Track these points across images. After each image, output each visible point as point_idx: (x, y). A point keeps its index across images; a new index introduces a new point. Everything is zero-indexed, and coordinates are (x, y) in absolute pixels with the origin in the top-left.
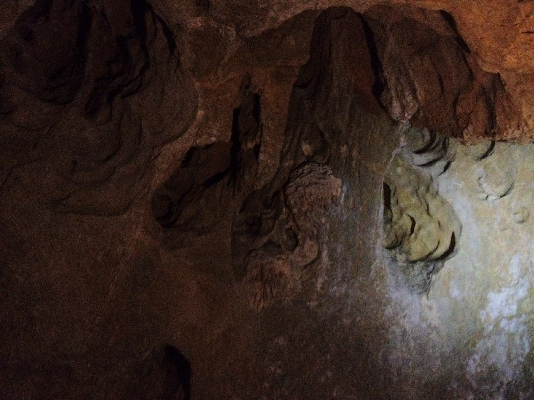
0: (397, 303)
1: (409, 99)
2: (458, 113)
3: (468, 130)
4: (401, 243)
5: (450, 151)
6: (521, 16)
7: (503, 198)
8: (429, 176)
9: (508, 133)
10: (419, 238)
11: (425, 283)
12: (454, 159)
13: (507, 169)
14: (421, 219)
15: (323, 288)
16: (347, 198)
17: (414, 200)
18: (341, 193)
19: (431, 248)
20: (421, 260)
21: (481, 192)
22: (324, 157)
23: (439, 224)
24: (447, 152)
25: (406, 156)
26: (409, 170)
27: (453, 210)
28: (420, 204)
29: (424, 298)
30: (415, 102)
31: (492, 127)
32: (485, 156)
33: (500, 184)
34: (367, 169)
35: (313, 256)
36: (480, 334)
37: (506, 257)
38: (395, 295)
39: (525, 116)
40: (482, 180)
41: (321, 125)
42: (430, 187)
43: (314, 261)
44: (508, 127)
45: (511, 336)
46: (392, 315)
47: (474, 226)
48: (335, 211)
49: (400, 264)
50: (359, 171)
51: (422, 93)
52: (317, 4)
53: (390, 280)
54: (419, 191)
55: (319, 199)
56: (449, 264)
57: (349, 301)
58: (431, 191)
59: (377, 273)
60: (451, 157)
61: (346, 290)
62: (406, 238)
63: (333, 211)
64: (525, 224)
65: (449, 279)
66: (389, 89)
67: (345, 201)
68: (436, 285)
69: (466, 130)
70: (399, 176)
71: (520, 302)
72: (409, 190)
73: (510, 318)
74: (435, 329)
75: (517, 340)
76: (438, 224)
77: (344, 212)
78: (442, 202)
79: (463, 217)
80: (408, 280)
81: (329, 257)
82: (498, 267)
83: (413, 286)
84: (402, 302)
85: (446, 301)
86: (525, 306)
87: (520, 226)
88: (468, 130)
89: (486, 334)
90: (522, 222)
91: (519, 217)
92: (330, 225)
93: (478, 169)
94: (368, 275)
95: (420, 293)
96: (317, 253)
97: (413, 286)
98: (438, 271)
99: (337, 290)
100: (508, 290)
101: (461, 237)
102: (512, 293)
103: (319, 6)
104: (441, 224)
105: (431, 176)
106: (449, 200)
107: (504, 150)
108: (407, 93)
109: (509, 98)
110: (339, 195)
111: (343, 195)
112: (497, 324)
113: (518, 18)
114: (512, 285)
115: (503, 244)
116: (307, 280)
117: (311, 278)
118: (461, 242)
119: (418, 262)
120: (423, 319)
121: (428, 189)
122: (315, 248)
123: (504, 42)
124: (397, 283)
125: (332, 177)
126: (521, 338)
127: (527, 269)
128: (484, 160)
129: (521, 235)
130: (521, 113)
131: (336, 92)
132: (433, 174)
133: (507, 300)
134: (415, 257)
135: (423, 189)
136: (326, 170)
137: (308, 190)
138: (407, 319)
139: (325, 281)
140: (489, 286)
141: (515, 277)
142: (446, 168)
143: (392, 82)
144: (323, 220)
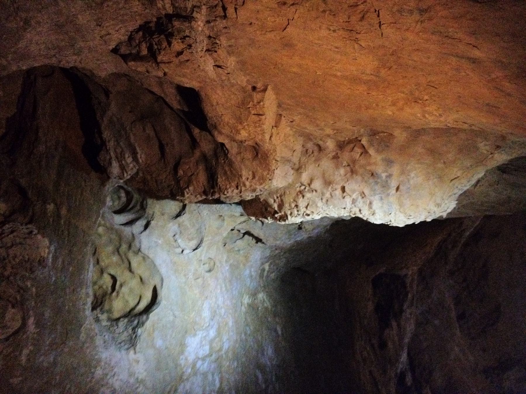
0: (106, 363)
1: (129, 160)
2: (179, 174)
3: (189, 190)
4: (101, 303)
5: (149, 211)
6: (253, 102)
7: (195, 251)
8: (130, 233)
9: (228, 192)
10: (121, 295)
11: (131, 338)
12: (152, 218)
13: (197, 226)
14: (122, 276)
15: (29, 360)
16: (55, 258)
17: (115, 259)
18: (49, 253)
19: (132, 304)
20: (125, 316)
21: (177, 247)
22: (25, 217)
23: (141, 279)
24: (145, 212)
25: (107, 215)
26: (110, 229)
27: (155, 265)
28: (120, 262)
29: (132, 352)
30: (135, 164)
31: (213, 187)
32: (178, 215)
33: (192, 239)
34: (77, 227)
35: (17, 325)
36: (181, 379)
37: (200, 303)
38: (104, 355)
39: (244, 178)
40: (177, 236)
41: (23, 182)
42: (133, 244)
43: (16, 332)
44: (228, 186)
45: (205, 375)
46: (102, 377)
47: (173, 278)
48: (42, 274)
49: (105, 323)
50: (68, 230)
51: (142, 156)
52: (60, 62)
53: (99, 341)
54: (120, 250)
55: (25, 261)
56: (153, 316)
57: (58, 369)
58: (133, 248)
59: (88, 335)
60: (150, 216)
61: (54, 359)
62: (108, 297)
63: (40, 273)
64: (213, 272)
65: (154, 331)
66: (107, 151)
67: (52, 263)
68: (142, 337)
69: (187, 190)
70: (100, 235)
71: (211, 342)
72: (110, 249)
73: (203, 359)
74: (141, 382)
75: (210, 377)
76: (139, 280)
77: (52, 273)
78: (144, 258)
79: (163, 270)
80: (113, 338)
81: (36, 324)
82: (194, 313)
83: (120, 343)
84: (110, 360)
85: (151, 352)
86: (216, 345)
87: (208, 274)
88: (189, 190)
89: (185, 378)
90: (210, 271)
91: (207, 267)
92: (36, 289)
93: (173, 227)
94: (78, 338)
95: (128, 349)
96: (20, 322)
97: (120, 343)
98: (143, 324)
99: (45, 360)
100: (201, 332)
101: (163, 289)
102: (204, 335)
103: (62, 63)
104: (143, 279)
105: (133, 235)
106: (151, 256)
107: (195, 210)
108: (127, 156)
109: (231, 164)
110: (46, 255)
111: (51, 255)
112: (194, 365)
113: (251, 103)
114: (204, 327)
115: (197, 291)
116: (10, 354)
117: (13, 351)
118: (162, 294)
119: (122, 319)
120: (131, 375)
121: (130, 247)
122: (19, 317)
123: (240, 120)
124: (105, 342)
125: (39, 237)
126: (213, 375)
127: (215, 311)
128: (178, 218)
129: (210, 282)
130: (241, 176)
131: (42, 148)
132: (134, 232)
133: (201, 342)
134: (116, 315)
135: (124, 247)
136: (31, 230)
137: (11, 252)
138: (116, 378)
139: (31, 351)
140: (186, 332)
141: (207, 320)
142: (146, 226)
143: (111, 144)
144: (29, 284)
